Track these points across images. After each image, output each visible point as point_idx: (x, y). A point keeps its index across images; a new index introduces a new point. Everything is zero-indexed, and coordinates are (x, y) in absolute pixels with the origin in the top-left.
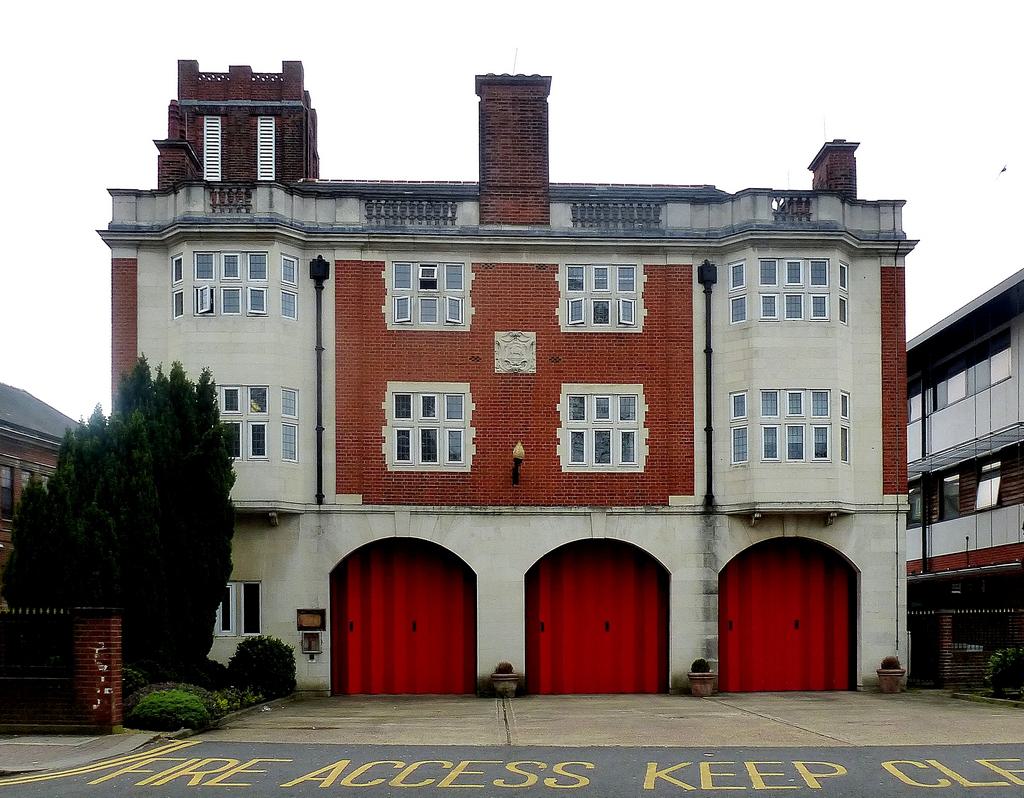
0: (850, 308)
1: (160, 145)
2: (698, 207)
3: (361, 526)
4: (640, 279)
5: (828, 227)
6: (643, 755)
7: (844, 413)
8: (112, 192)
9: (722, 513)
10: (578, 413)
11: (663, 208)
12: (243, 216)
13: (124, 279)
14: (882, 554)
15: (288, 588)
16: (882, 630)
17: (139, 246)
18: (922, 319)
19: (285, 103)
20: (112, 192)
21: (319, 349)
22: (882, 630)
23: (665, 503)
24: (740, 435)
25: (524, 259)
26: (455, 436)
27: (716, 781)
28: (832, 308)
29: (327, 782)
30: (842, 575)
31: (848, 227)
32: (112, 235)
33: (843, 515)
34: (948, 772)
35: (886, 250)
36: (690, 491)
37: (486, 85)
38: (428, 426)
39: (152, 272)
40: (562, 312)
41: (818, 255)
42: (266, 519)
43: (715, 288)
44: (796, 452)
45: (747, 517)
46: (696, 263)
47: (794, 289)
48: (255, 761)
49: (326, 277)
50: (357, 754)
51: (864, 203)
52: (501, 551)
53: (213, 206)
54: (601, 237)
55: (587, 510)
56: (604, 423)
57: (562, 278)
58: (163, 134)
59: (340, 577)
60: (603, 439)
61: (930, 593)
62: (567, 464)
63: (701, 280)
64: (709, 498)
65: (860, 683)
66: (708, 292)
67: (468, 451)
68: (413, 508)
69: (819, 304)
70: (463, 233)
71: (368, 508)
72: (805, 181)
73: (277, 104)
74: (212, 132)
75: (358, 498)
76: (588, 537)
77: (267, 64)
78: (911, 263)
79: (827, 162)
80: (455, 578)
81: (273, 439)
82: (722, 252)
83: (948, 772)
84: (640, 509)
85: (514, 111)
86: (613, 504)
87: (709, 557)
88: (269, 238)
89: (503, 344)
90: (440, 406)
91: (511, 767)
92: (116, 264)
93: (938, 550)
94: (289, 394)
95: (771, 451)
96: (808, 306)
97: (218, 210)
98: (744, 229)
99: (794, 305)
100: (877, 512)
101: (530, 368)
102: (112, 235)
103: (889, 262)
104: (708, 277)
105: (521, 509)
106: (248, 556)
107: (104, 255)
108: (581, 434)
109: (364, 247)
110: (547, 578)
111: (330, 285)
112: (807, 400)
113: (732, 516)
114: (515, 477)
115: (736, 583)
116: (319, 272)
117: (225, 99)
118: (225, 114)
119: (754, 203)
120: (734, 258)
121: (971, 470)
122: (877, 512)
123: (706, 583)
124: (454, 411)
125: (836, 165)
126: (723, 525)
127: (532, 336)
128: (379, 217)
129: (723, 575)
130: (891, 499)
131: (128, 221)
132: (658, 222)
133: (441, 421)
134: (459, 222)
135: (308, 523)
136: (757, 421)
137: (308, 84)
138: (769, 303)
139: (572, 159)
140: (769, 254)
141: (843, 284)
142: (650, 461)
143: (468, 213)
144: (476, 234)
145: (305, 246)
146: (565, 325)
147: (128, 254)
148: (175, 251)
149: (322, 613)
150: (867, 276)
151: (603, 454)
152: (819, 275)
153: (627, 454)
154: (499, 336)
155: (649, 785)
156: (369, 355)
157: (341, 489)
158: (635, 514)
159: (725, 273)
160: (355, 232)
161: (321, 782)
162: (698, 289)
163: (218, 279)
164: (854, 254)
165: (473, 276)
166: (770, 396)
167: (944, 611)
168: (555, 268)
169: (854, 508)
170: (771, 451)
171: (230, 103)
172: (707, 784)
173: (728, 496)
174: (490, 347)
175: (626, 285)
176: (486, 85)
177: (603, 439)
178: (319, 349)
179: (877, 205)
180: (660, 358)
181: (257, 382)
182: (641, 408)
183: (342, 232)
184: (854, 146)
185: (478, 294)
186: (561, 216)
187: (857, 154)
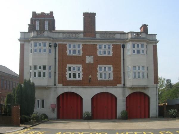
1: (29, 25)
3: (62, 90)
4: (111, 47)
17: (25, 41)
30: (146, 98)
31: (147, 38)
36: (121, 84)
41: (70, 43)
44: (139, 77)
49: (57, 46)
52: (87, 94)
53: (38, 35)
56: (105, 72)
59: (58, 98)
60: (74, 74)
63: (122, 47)
64: (124, 85)
65: (150, 117)
66: (123, 49)
67: (112, 77)
68: (106, 87)
71: (63, 86)
74: (38, 23)
75: (62, 85)
78: (158, 44)
80: (78, 99)
84: (112, 87)
85: (89, 19)
92: (21, 44)
100: (153, 87)
101: (92, 62)
103: (154, 44)
104: (123, 46)
107: (19, 43)
109: (63, 41)
110: (95, 99)
111: (57, 48)
115: (129, 99)
117: (40, 18)
118: (40, 20)
122: (153, 87)
127: (92, 57)
133: (76, 71)
135: (53, 89)
137: (54, 15)
139: (100, 26)
142: (114, 78)
147: (23, 43)
149: (56, 104)
150: (151, 47)
151: (74, 77)
156: (64, 60)
157: (59, 83)
162: (122, 49)
163: (136, 48)
168: (97, 45)
176: (96, 13)
179: (152, 35)
180: (116, 61)
181: (44, 64)
182: (112, 69)
186: (98, 36)
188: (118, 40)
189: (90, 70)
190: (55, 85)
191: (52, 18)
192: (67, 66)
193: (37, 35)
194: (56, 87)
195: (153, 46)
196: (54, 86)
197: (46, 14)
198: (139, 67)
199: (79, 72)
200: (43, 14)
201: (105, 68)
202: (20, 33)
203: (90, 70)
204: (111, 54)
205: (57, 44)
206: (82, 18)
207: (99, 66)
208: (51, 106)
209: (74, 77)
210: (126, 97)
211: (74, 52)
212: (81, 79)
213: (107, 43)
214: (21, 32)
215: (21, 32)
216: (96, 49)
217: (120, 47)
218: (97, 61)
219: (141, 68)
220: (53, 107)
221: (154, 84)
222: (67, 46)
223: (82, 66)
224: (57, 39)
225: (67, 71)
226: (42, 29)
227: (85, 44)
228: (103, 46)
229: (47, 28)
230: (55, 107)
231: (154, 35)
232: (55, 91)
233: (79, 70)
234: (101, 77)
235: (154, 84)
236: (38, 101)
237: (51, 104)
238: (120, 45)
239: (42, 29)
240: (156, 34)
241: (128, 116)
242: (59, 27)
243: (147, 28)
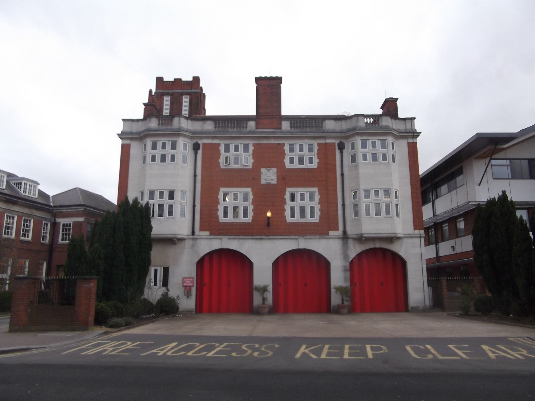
0: (396, 158)
1: (145, 104)
2: (337, 121)
3: (208, 244)
4: (316, 148)
5: (387, 128)
6: (298, 341)
7: (396, 198)
8: (123, 120)
9: (351, 238)
10: (293, 198)
11: (324, 122)
12: (169, 127)
13: (125, 152)
14: (416, 255)
15: (180, 269)
16: (418, 288)
17: (131, 139)
18: (426, 163)
19: (193, 91)
20: (123, 120)
21: (195, 176)
22: (418, 288)
23: (328, 234)
24: (356, 206)
25: (272, 141)
26: (312, 209)
27: (350, 354)
28: (389, 158)
29: (161, 353)
30: (399, 264)
31: (394, 127)
32: (122, 136)
33: (399, 238)
34: (433, 351)
35: (411, 135)
36: (337, 229)
37: (258, 80)
38: (161, 203)
39: (135, 149)
40: (287, 161)
41: (228, 142)
42: (171, 241)
43: (345, 151)
44: (378, 213)
45: (360, 239)
46: (337, 142)
47: (374, 150)
48: (226, 344)
49: (199, 149)
50: (181, 339)
51: (400, 119)
52: (263, 255)
53: (159, 125)
54: (302, 133)
55: (297, 237)
56: (303, 203)
57: (287, 148)
58: (146, 101)
59: (200, 263)
60: (302, 210)
61: (436, 271)
62: (289, 219)
63: (339, 148)
64: (345, 232)
65: (410, 308)
66: (341, 153)
67: (251, 214)
68: (229, 237)
69: (384, 157)
70: (249, 133)
71: (212, 237)
72: (380, 112)
73: (190, 91)
74: (167, 100)
75: (208, 233)
76: (220, 247)
77: (187, 77)
78: (419, 140)
79: (386, 105)
80: (243, 263)
81: (177, 210)
82: (347, 138)
83: (433, 351)
84: (317, 237)
85: (269, 89)
86: (306, 235)
87: (345, 256)
88: (178, 135)
89: (264, 173)
90: (307, 196)
91: (244, 347)
92: (123, 146)
93: (442, 253)
94: (183, 192)
95: (368, 213)
96: (380, 157)
97: (160, 126)
98: (354, 129)
99: (375, 157)
100: (412, 237)
101: (274, 182)
102: (122, 136)
103: (411, 140)
104: (341, 147)
105: (271, 237)
106: (157, 254)
107: (119, 142)
108: (227, 207)
109: (213, 138)
110: (281, 264)
111: (200, 152)
112: (381, 193)
113: (354, 239)
114: (268, 225)
115: (355, 267)
116: (196, 147)
117: (172, 90)
118: (171, 95)
119: (358, 119)
120: (352, 140)
121: (452, 220)
122: (412, 237)
123: (345, 267)
124: (311, 198)
125: (390, 106)
126: (351, 243)
127: (275, 170)
128: (219, 127)
129: (352, 263)
130: (417, 232)
131: (128, 130)
132: (322, 127)
133: (236, 202)
134: (248, 129)
135: (188, 243)
136: (363, 202)
137: (202, 85)
138: (365, 157)
139: (291, 105)
140: (364, 138)
141: (393, 149)
142: (321, 217)
143: (252, 125)
144: (254, 132)
145: (191, 138)
146: (288, 165)
147: (127, 142)
148: (144, 141)
149: (193, 278)
150: (402, 146)
151: (303, 215)
152: (384, 146)
153: (312, 215)
154: (263, 170)
155: (298, 355)
156: (213, 178)
157: (201, 229)
158: (315, 239)
159: (348, 146)
160: (209, 133)
161: (159, 353)
162: (338, 152)
163: (159, 152)
164: (397, 137)
165: (318, 148)
166: (367, 191)
167: (442, 278)
168: (284, 145)
169: (402, 236)
170: (368, 213)
171: (174, 91)
172: (346, 356)
173: (351, 231)
174: (259, 174)
175: (311, 150)
176: (258, 80)
177: (302, 210)
178: (195, 176)
179: (405, 119)
180: (324, 178)
181: (171, 188)
182: (317, 197)
183: (205, 133)
184: (397, 100)
185: (254, 155)
186: (286, 126)
187: (397, 102)
188: (332, 134)
189: (268, 197)
190: (193, 233)
191: (198, 91)
192: (285, 191)
193: (157, 126)
194: (196, 239)
195: (409, 143)
196: (192, 237)
197: (185, 81)
198: (161, 194)
199: (313, 203)
200: (178, 81)
201: (302, 195)
202: (122, 122)
203: (268, 197)
204: (315, 165)
205: (199, 145)
206: (254, 86)
207: (223, 190)
208: (184, 282)
209: (303, 215)
210: (350, 261)
211: (301, 161)
212: (249, 219)
213: (306, 141)
214: (124, 120)
215: (124, 120)
216: (283, 154)
217: (335, 149)
218: (284, 179)
219: (381, 193)
220: (188, 283)
221: (414, 229)
222: (220, 148)
223: (252, 190)
224: (201, 133)
225: (287, 203)
226: (176, 111)
227: (258, 144)
228: (297, 147)
229: (185, 111)
230: (191, 284)
231: (410, 121)
232: (193, 246)
233: (245, 199)
234: (293, 216)
235: (414, 229)
236: (156, 271)
237: (183, 278)
238: (334, 143)
239: (176, 111)
240: (415, 118)
241: (282, 306)
242: (212, 108)
243: (397, 104)
